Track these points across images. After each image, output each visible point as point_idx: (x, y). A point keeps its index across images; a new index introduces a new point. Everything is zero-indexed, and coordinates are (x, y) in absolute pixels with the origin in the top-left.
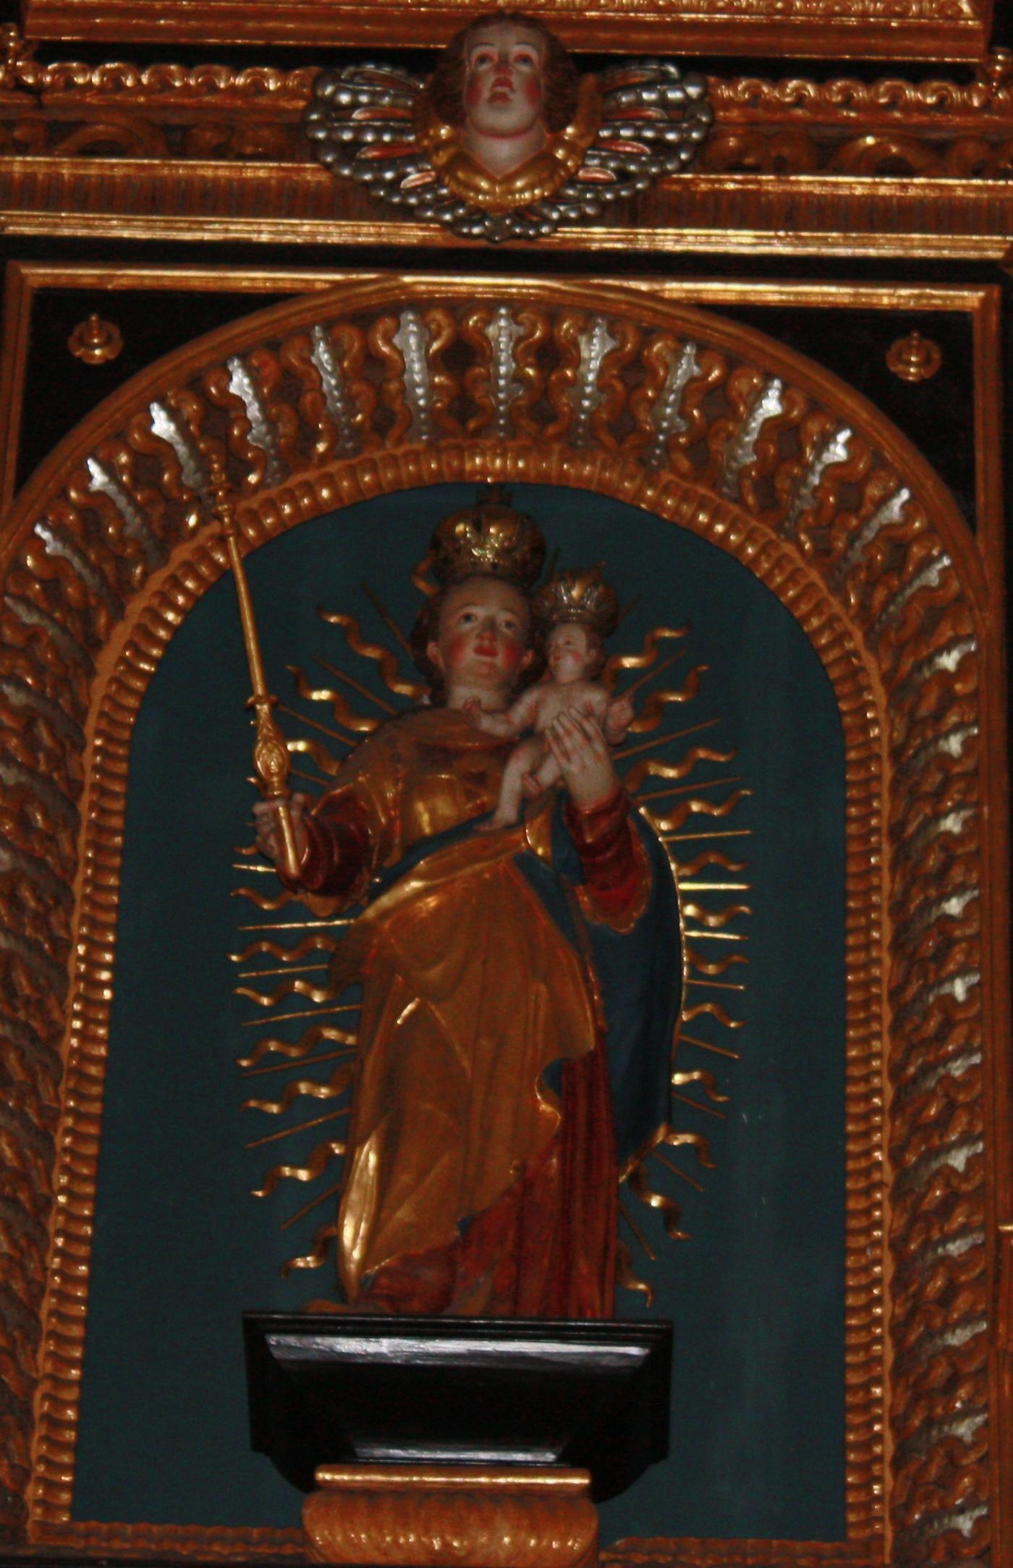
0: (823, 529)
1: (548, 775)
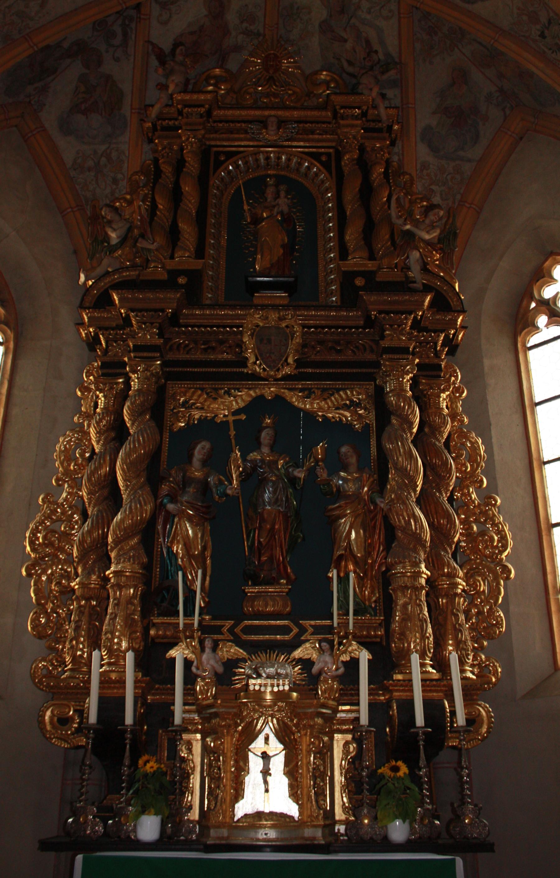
1: (280, 209)
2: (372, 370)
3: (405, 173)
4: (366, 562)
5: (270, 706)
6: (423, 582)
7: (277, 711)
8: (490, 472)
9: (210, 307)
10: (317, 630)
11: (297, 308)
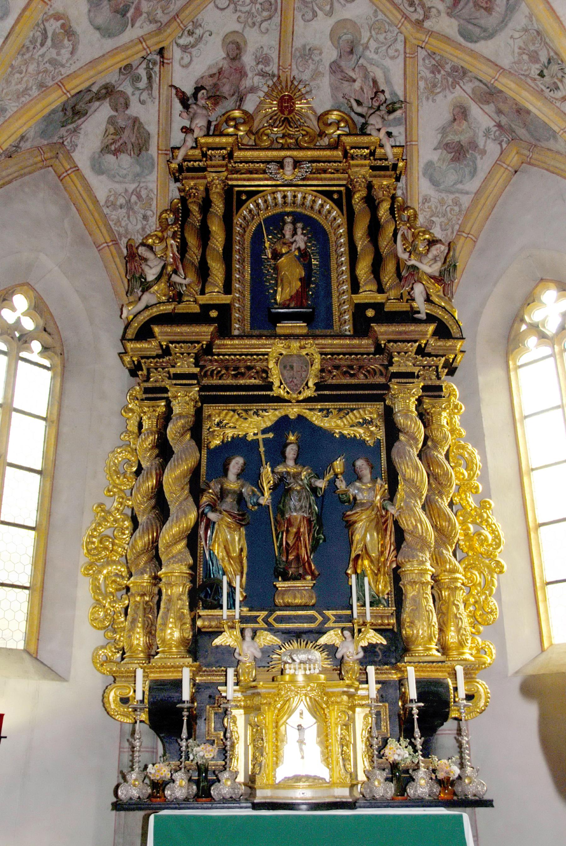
0: (326, 217)
2: (382, 392)
3: (408, 208)
4: (379, 560)
5: (304, 687)
6: (428, 578)
7: (310, 690)
8: (484, 478)
9: (239, 337)
10: (339, 619)
11: (316, 337)
